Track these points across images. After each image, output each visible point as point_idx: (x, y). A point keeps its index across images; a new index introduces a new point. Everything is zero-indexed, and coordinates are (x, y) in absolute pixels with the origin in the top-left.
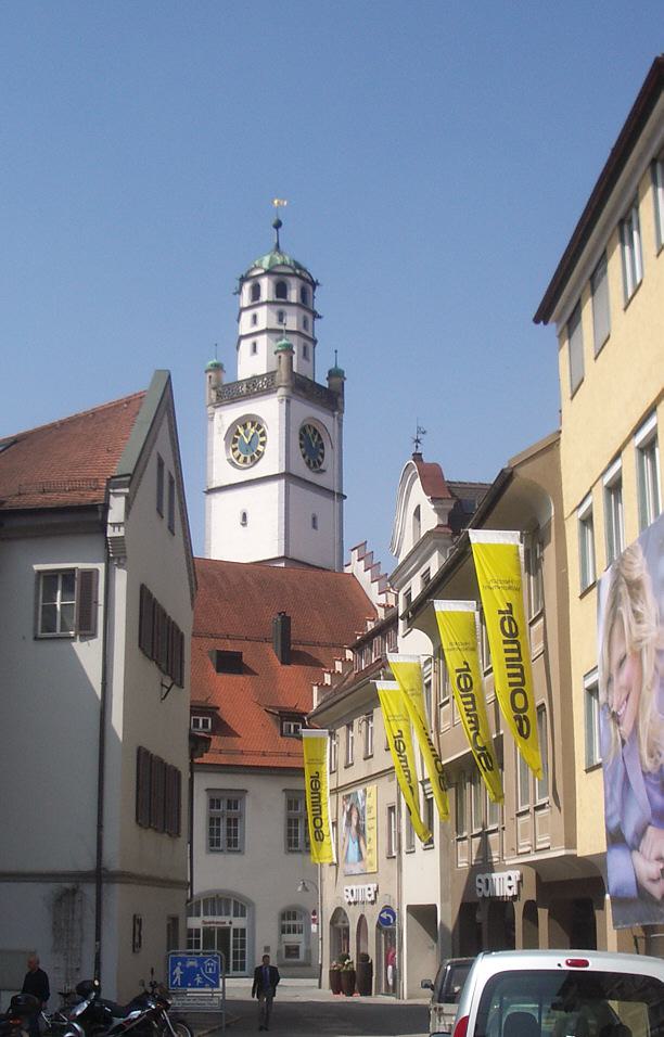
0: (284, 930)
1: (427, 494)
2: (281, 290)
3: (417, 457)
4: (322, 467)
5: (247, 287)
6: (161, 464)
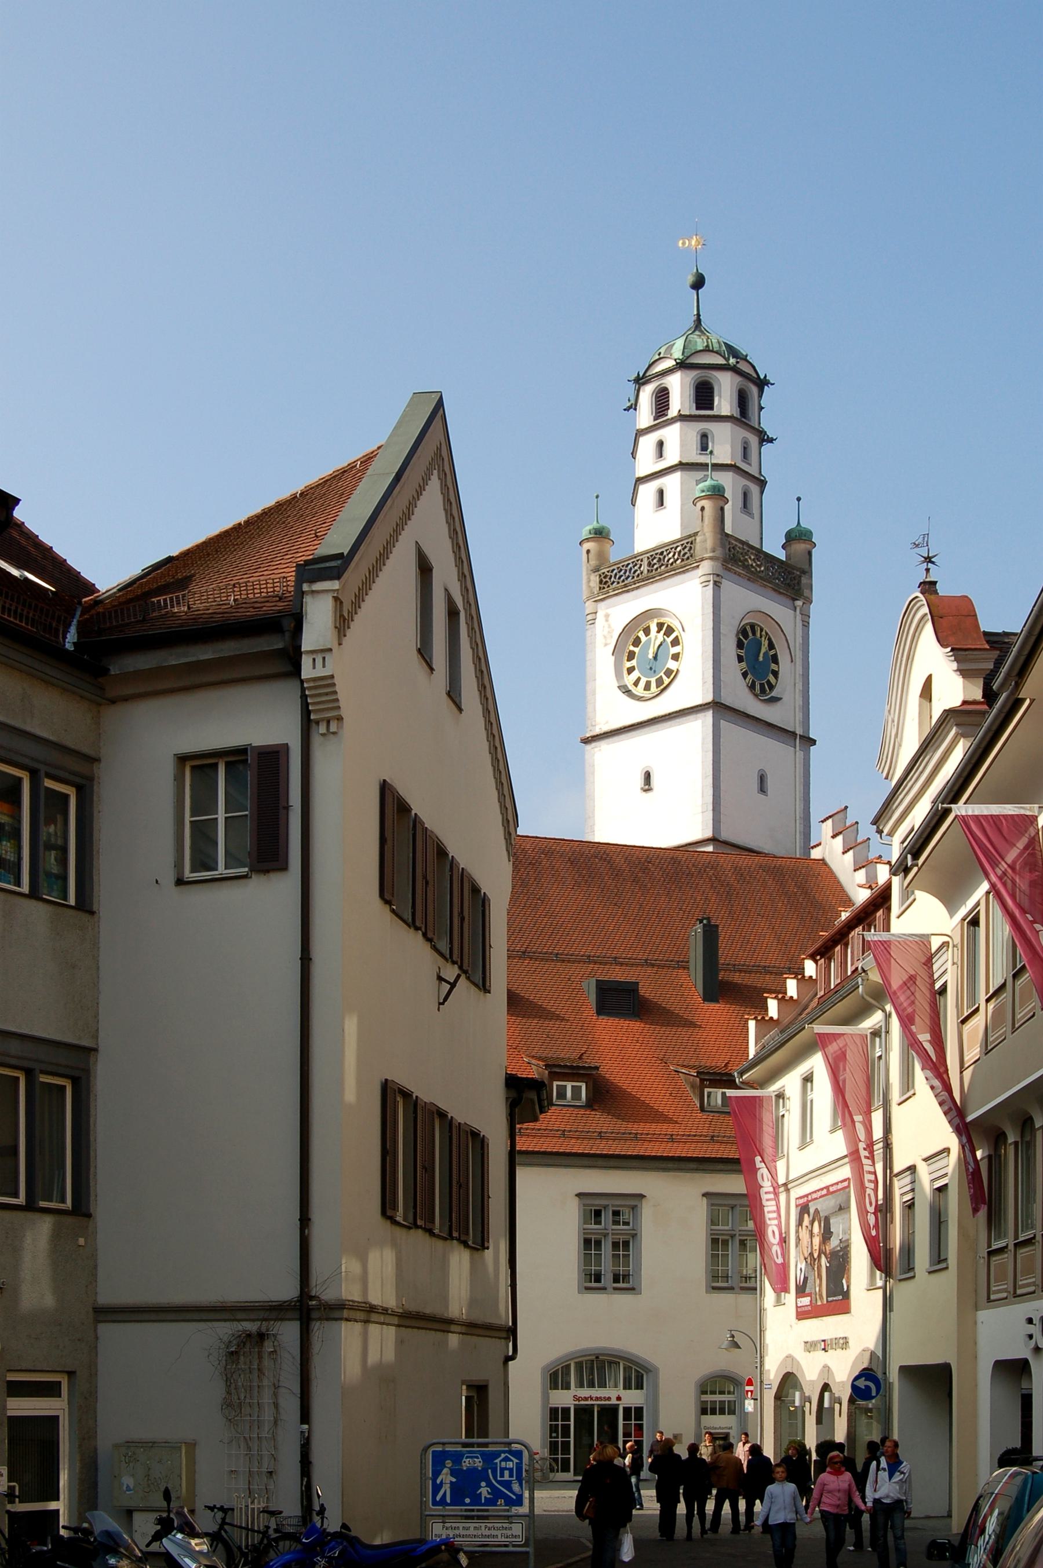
0: (705, 1410)
1: (943, 645)
2: (704, 395)
3: (928, 587)
4: (774, 694)
5: (647, 393)
6: (425, 569)
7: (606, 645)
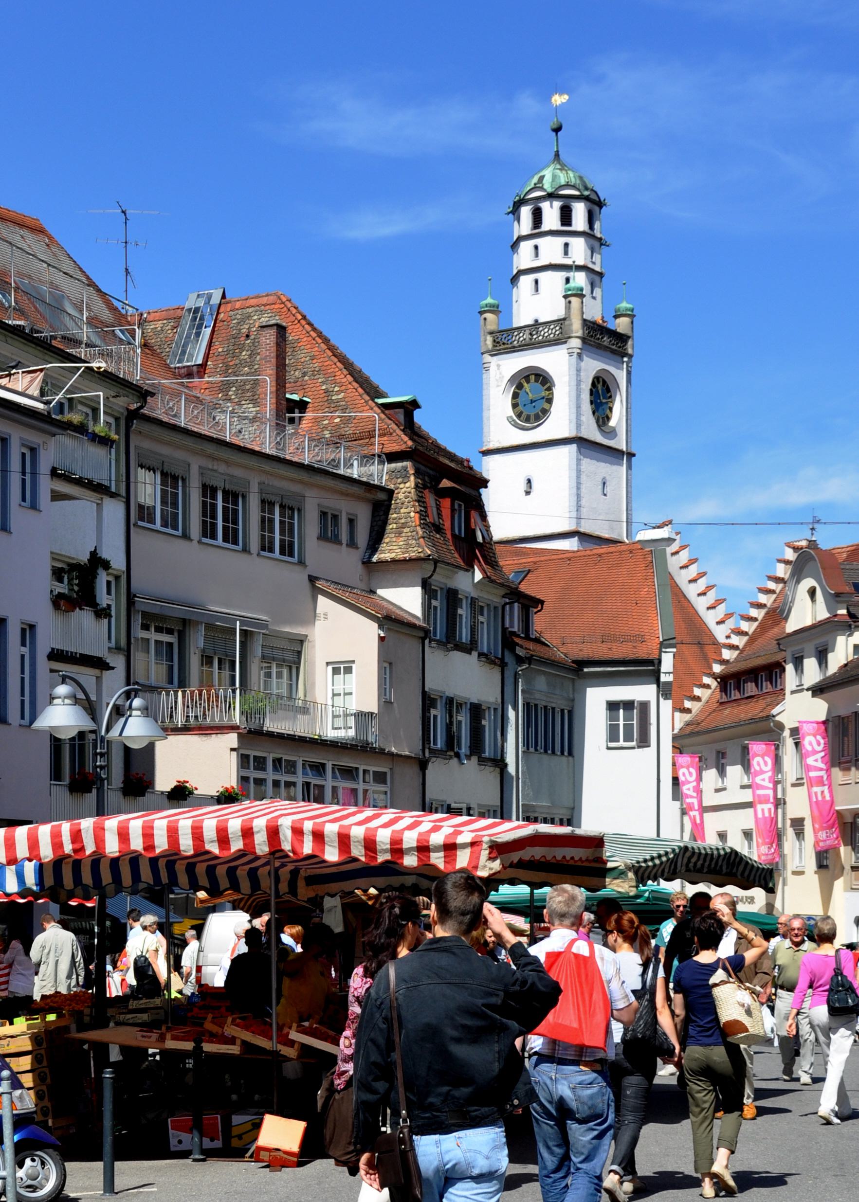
2: (566, 216)
5: (526, 212)
7: (498, 386)
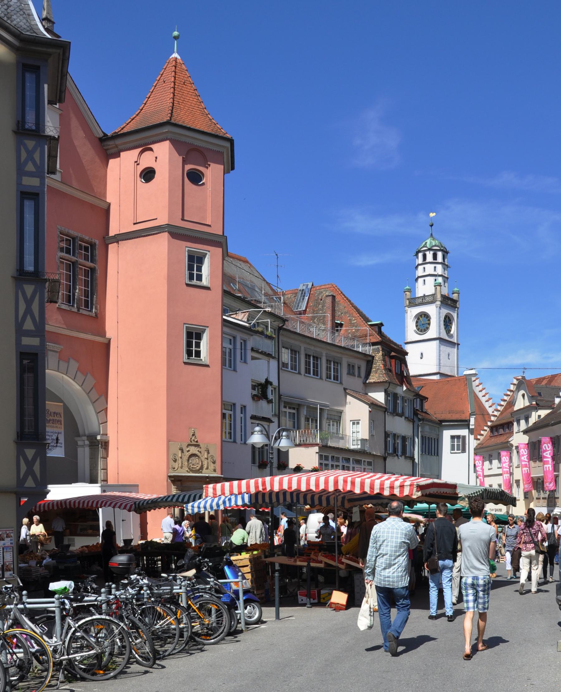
5: (420, 255)
